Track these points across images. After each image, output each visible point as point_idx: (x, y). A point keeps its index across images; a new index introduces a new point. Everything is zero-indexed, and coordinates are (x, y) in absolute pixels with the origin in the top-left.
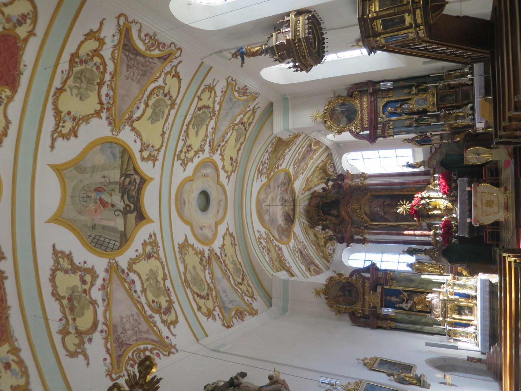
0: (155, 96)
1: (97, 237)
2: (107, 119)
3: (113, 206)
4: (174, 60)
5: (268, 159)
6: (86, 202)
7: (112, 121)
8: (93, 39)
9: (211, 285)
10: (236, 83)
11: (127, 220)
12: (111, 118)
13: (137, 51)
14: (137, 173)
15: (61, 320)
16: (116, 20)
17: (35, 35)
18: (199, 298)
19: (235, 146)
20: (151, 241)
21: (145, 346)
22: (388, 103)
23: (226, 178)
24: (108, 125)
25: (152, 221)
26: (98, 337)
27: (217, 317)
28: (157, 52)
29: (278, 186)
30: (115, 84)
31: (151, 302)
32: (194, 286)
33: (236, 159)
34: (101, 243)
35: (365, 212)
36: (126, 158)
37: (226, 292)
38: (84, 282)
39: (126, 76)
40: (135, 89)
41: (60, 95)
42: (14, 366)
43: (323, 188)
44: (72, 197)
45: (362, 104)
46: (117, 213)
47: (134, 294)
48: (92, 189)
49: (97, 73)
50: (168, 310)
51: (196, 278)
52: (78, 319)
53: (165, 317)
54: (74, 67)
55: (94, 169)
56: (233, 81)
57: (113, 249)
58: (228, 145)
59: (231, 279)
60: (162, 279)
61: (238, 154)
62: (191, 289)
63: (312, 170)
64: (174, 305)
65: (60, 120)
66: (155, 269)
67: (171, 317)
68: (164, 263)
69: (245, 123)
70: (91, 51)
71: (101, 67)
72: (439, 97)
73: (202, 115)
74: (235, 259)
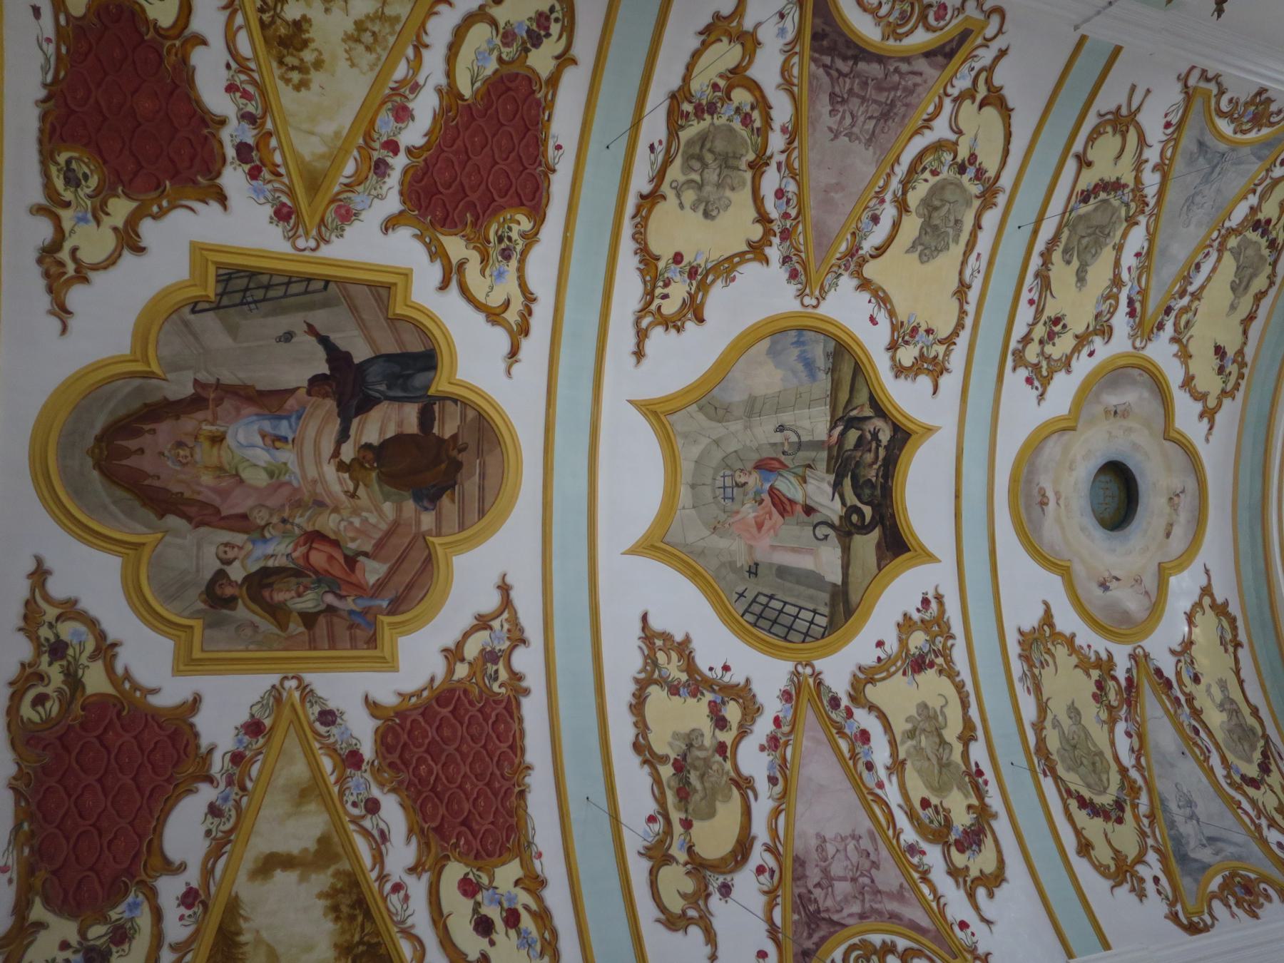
0: (927, 175)
1: (763, 600)
2: (784, 263)
3: (809, 510)
4: (980, 52)
6: (733, 499)
7: (798, 267)
8: (725, 40)
9: (1134, 774)
10: (1219, 84)
12: (795, 258)
13: (857, 46)
14: (880, 412)
15: (651, 819)
17: (574, 62)
18: (1084, 812)
19: (1233, 307)
20: (927, 617)
21: (888, 938)
23: (1201, 416)
24: (789, 282)
25: (930, 558)
26: (746, 883)
27: (1150, 886)
28: (920, 38)
30: (800, 157)
31: (917, 805)
32: (1069, 769)
33: (1240, 352)
34: (773, 615)
36: (846, 370)
37: (1190, 803)
38: (721, 723)
39: (830, 129)
40: (863, 163)
41: (650, 211)
42: (527, 922)
44: (693, 486)
46: (822, 531)
47: (865, 774)
48: (750, 465)
50: (973, 838)
51: (1077, 746)
52: (697, 824)
53: (959, 859)
54: (682, 127)
55: (753, 408)
56: (1208, 80)
57: (806, 634)
58: (1203, 306)
59: (1215, 760)
60: (959, 738)
61: (1245, 333)
62: (1057, 778)
64: (994, 824)
65: (655, 279)
66: (935, 704)
67: (983, 861)
68: (969, 687)
69: (1268, 221)
70: (721, 76)
73: (1094, 216)
74: (1236, 694)
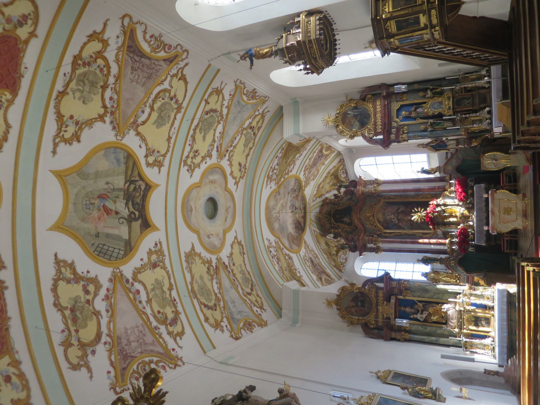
0: (161, 99)
1: (101, 246)
2: (111, 123)
3: (117, 213)
4: (180, 63)
5: (277, 164)
6: (89, 209)
7: (116, 125)
8: (97, 41)
9: (219, 295)
10: (244, 85)
11: (132, 228)
12: (115, 122)
13: (142, 53)
14: (142, 179)
15: (63, 331)
16: (120, 21)
17: (36, 36)
18: (206, 308)
19: (244, 151)
20: (157, 249)
21: (150, 358)
22: (402, 106)
23: (235, 184)
24: (112, 130)
25: (157, 229)
26: (101, 349)
27: (225, 328)
28: (162, 54)
29: (289, 193)
30: (119, 87)
31: (156, 313)
32: (201, 296)
33: (245, 165)
34: (104, 251)
35: (378, 220)
36: (131, 164)
37: (234, 302)
38: (87, 292)
39: (131, 79)
40: (140, 92)
41: (62, 98)
42: (14, 379)
43: (335, 195)
44: (74, 204)
45: (375, 107)
46: (122, 220)
47: (139, 305)
48: (96, 196)
49: (100, 75)
50: (174, 321)
51: (203, 288)
52: (80, 331)
53: (171, 329)
54: (77, 69)
55: (97, 175)
56: (242, 84)
57: (117, 258)
58: (236, 150)
59: (240, 289)
60: (168, 289)
61: (246, 159)
62: (198, 299)
63: (324, 176)
64: (180, 316)
65: (62, 124)
66: (160, 279)
67: (177, 329)
68: (170, 272)
69: (254, 127)
70: (94, 53)
71: (105, 69)
72: (455, 101)
73: (209, 119)
74: (244, 268)
